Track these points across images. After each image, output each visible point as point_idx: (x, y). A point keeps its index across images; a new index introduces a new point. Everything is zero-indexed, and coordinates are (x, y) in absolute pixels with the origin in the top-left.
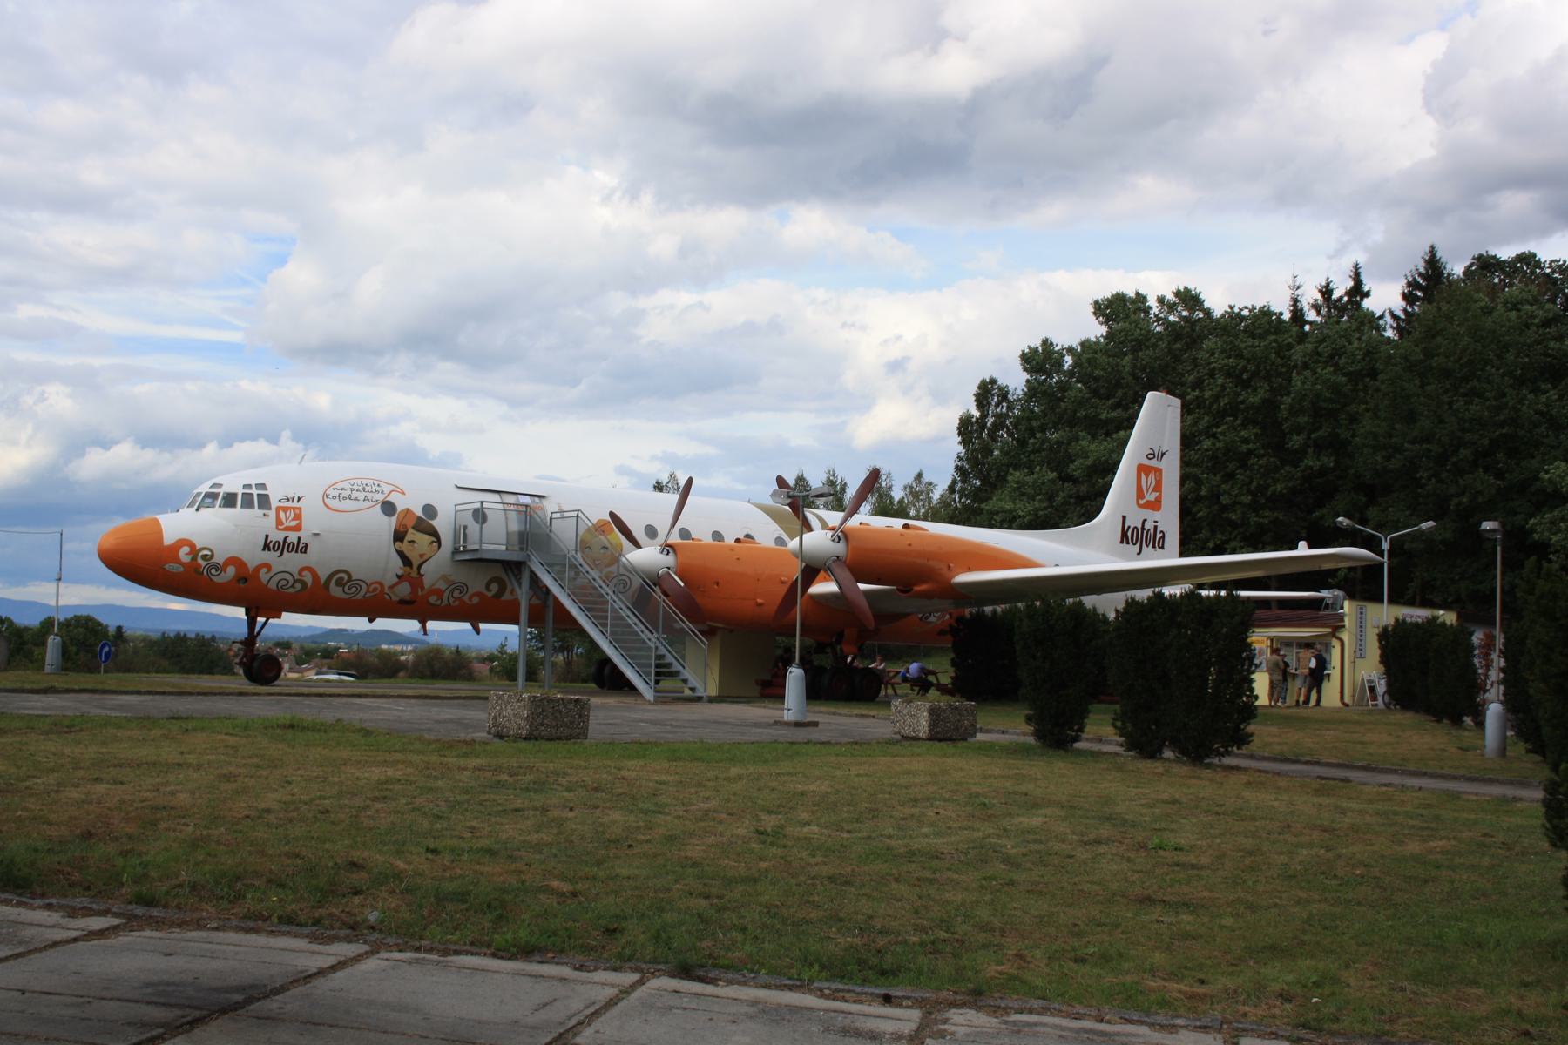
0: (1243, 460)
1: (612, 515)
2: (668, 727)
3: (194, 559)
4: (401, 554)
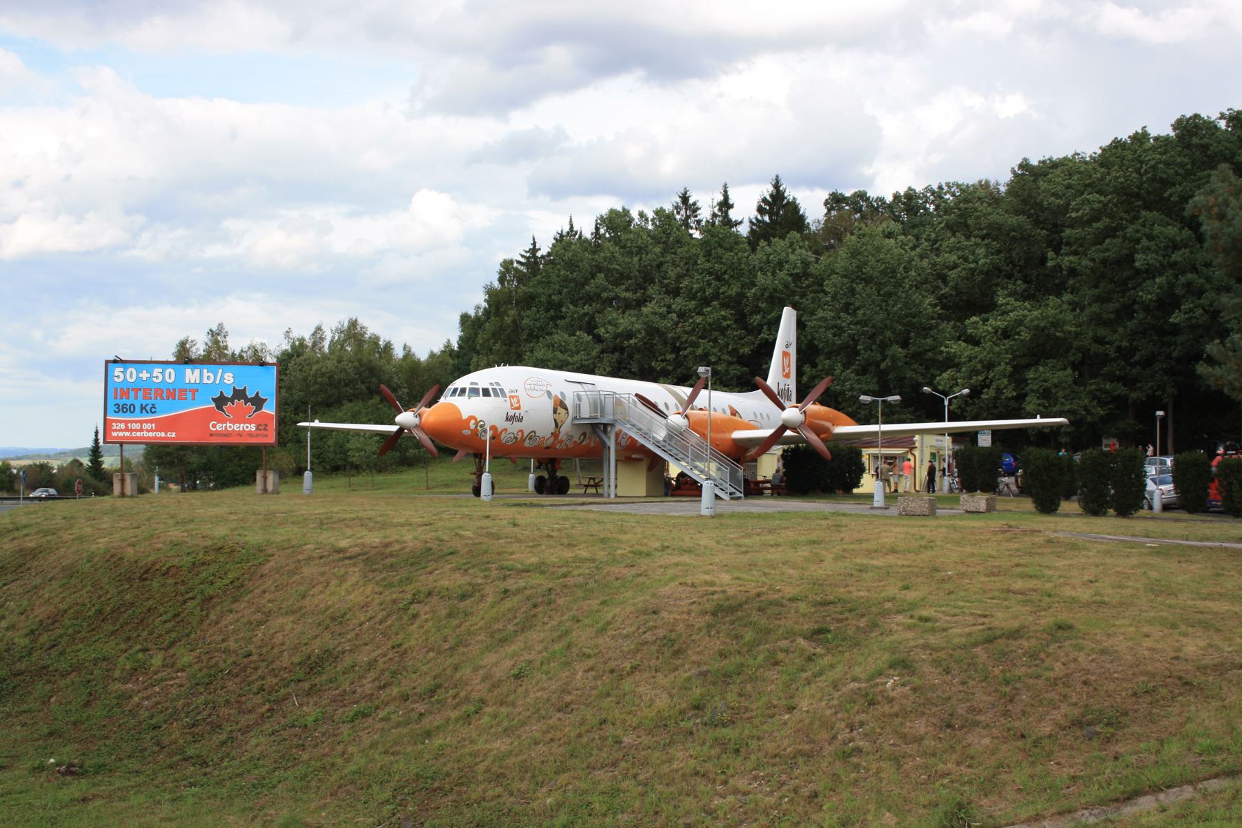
0: (723, 331)
1: (637, 395)
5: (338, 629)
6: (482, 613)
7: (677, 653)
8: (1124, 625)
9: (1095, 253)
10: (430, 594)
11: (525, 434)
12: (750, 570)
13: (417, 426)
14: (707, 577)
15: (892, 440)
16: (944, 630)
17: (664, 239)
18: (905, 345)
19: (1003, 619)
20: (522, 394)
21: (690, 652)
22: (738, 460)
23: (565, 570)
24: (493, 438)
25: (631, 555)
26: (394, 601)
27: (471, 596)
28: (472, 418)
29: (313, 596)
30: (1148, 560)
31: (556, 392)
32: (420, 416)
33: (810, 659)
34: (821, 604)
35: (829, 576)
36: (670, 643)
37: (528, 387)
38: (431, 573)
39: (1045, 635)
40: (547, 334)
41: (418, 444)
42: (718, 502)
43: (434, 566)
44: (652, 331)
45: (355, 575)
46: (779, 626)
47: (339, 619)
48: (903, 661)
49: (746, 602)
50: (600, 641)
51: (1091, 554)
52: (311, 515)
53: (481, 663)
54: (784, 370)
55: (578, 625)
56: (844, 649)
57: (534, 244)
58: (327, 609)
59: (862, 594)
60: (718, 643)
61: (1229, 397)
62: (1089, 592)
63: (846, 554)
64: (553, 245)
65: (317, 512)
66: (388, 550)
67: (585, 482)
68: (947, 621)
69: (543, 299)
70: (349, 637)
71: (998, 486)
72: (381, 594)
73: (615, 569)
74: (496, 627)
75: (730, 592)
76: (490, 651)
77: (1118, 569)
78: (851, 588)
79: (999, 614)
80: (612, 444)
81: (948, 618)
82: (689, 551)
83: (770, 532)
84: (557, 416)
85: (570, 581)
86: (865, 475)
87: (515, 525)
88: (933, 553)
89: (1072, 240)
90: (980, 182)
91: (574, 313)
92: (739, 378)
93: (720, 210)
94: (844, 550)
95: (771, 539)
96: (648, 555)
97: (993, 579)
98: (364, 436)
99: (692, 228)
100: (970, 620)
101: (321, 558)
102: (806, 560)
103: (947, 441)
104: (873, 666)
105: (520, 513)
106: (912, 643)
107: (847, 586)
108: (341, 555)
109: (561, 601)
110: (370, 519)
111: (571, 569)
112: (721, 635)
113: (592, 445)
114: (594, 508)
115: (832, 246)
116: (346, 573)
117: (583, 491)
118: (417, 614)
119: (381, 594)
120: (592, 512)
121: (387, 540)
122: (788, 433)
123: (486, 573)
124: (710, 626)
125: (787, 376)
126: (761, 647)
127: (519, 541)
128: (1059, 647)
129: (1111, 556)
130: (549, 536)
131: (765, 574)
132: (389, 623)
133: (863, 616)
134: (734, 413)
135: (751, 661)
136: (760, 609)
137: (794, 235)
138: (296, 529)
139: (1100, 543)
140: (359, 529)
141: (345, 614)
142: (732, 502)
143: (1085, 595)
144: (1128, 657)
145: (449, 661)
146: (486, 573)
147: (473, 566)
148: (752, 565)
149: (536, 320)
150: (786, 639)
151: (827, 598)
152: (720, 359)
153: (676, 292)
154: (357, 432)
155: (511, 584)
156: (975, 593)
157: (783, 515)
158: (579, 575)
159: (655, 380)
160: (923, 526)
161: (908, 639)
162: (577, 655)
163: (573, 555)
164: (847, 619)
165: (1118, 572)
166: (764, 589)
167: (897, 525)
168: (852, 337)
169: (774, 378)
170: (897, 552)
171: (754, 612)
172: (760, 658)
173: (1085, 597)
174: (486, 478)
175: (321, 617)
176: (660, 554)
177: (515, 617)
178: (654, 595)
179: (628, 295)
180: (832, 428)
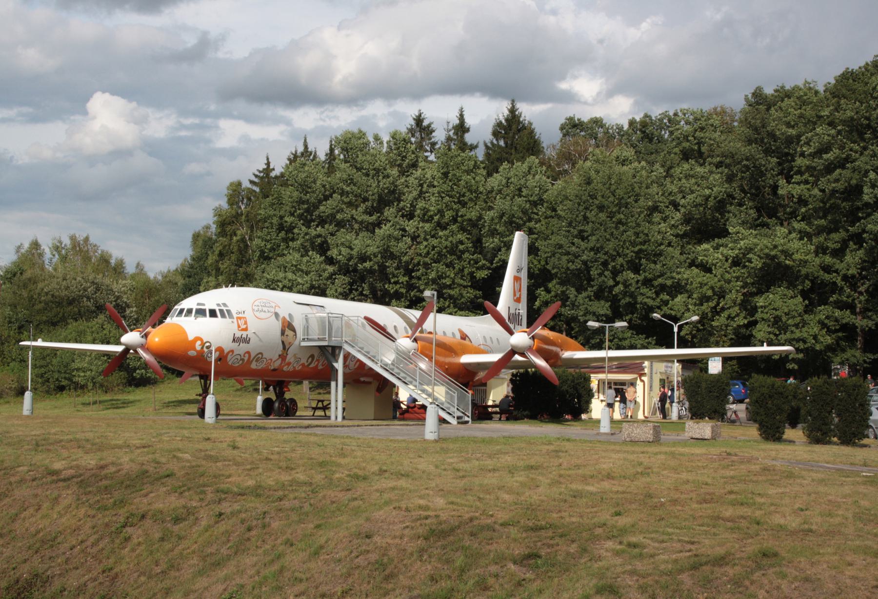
1: (366, 318)
2: (319, 433)
3: (202, 348)
4: (283, 342)
5: (48, 553)
6: (195, 536)
7: (387, 578)
8: (828, 554)
9: (828, 183)
10: (143, 517)
11: (253, 356)
12: (465, 495)
13: (142, 346)
14: (422, 502)
15: (624, 366)
16: (652, 556)
17: (398, 162)
18: (636, 269)
19: (710, 547)
20: (249, 316)
21: (401, 577)
22: (466, 385)
23: (281, 493)
24: (219, 359)
25: (348, 479)
26: (107, 525)
27: (184, 520)
28: (198, 339)
29: (24, 519)
30: (862, 489)
31: (284, 313)
32: (146, 336)
33: (519, 584)
34: (532, 529)
35: (543, 501)
36: (382, 567)
37: (256, 308)
38: (146, 495)
39: (750, 563)
40: (279, 255)
41: (146, 365)
42: (445, 425)
43: (149, 490)
44: (387, 253)
45: (68, 497)
46: (490, 551)
47: (51, 542)
48: (611, 587)
49: (459, 527)
50: (312, 565)
51: (806, 482)
52: (27, 436)
53: (193, 587)
54: (515, 295)
55: (291, 549)
56: (553, 574)
57: (268, 164)
58: (38, 532)
59: (574, 520)
60: (429, 567)
61: (288, 371)
62: (798, 520)
63: (562, 480)
64: (287, 165)
65: (33, 433)
66: (104, 472)
67: (314, 405)
68: (654, 548)
69: (275, 220)
70: (59, 560)
71: (726, 414)
72: (94, 517)
73: (331, 493)
74: (209, 551)
75: (444, 516)
76: (202, 576)
77: (830, 497)
78: (563, 514)
79: (707, 541)
80: (339, 365)
81: (656, 545)
82: (406, 475)
83: (490, 456)
84: (284, 338)
85: (286, 504)
86: (593, 400)
87: (235, 447)
88: (648, 480)
89: (803, 169)
90: (715, 109)
91: (306, 234)
92: (472, 301)
93: (456, 133)
94: (560, 476)
95: (490, 464)
96: (365, 478)
97: (705, 505)
98: (90, 356)
99: (427, 151)
100: (678, 546)
101: (33, 480)
102: (523, 485)
103: (677, 367)
104: (581, 592)
105: (241, 436)
106: (619, 569)
107: (560, 511)
108: (55, 478)
109: (275, 525)
110: (88, 440)
111: (286, 492)
112: (433, 560)
113: (320, 367)
114: (318, 431)
115: (566, 171)
116: (59, 496)
117: (312, 413)
118: (129, 538)
119: (94, 517)
120: (316, 435)
121: (102, 462)
122: (517, 357)
123: (202, 496)
124: (422, 551)
125: (518, 300)
126: (472, 572)
127: (237, 464)
128: (763, 575)
129: (826, 485)
130: (267, 459)
131: (480, 499)
132: (101, 546)
133: (573, 541)
134: (464, 337)
135: (461, 586)
136: (472, 534)
137: (533, 160)
138: (10, 450)
139: (817, 472)
140: (75, 450)
141: (56, 537)
142: (460, 426)
143: (794, 523)
144: (831, 586)
145: (160, 586)
146: (202, 496)
147: (189, 489)
148: (467, 490)
149: (267, 241)
150: (496, 563)
151: (539, 523)
152: (453, 283)
153: (410, 216)
154: (83, 353)
155: (226, 507)
156: (686, 519)
157: (508, 439)
158: (295, 498)
159: (387, 304)
160: (643, 453)
161: (616, 566)
162: (289, 579)
163: (290, 478)
164: (558, 545)
165: (830, 501)
166: (477, 514)
167: (618, 452)
168: (585, 263)
169: (502, 306)
170: (613, 478)
171: (466, 537)
172: (471, 582)
173: (794, 525)
174: (210, 401)
175: (31, 541)
176: (377, 478)
177: (229, 541)
178: (368, 519)
179: (366, 218)
180: (561, 353)
